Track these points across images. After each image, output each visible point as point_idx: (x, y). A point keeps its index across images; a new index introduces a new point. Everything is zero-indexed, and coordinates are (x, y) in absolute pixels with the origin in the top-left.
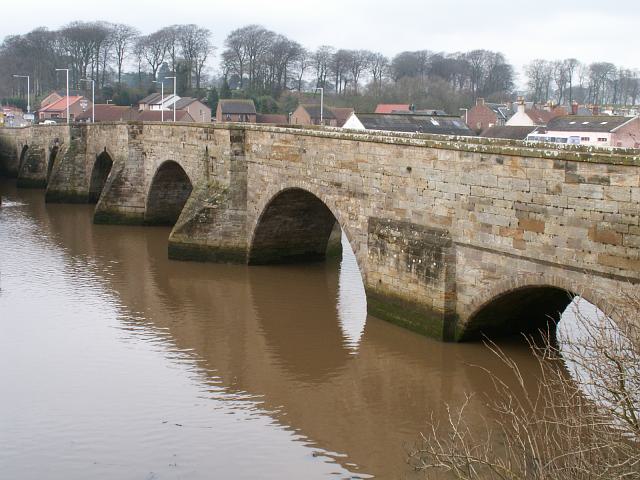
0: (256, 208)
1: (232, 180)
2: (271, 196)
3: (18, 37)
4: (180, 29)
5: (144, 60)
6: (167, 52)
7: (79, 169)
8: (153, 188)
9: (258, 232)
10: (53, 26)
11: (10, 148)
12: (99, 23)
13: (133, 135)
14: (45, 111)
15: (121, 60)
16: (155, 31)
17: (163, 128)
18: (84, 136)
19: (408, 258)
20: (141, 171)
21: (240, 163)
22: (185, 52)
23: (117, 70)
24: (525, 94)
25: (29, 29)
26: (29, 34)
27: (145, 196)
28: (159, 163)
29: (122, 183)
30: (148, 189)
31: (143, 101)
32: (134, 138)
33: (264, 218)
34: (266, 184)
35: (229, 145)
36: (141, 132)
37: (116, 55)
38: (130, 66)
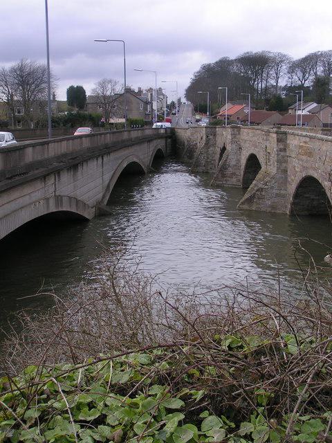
0: (292, 188)
1: (278, 168)
2: (298, 181)
3: (209, 65)
4: (321, 54)
5: (295, 77)
6: (312, 72)
7: (211, 158)
8: (245, 173)
9: (293, 204)
10: (232, 57)
11: (181, 142)
12: (263, 52)
13: (234, 135)
14: (220, 116)
15: (278, 78)
16: (304, 56)
17: (250, 131)
18: (215, 135)
19: (192, 382)
20: (239, 161)
21: (283, 157)
22: (324, 71)
23: (275, 84)
24: (202, 311)
25: (217, 59)
26: (216, 62)
27: (241, 178)
28: (248, 154)
29: (226, 169)
30: (242, 173)
31: (292, 107)
32: (235, 137)
33: (296, 196)
34: (297, 172)
35: (275, 144)
36: (239, 134)
37: (275, 75)
38: (283, 82)
